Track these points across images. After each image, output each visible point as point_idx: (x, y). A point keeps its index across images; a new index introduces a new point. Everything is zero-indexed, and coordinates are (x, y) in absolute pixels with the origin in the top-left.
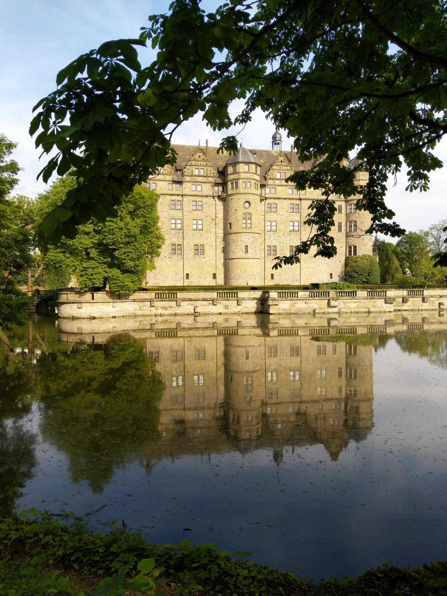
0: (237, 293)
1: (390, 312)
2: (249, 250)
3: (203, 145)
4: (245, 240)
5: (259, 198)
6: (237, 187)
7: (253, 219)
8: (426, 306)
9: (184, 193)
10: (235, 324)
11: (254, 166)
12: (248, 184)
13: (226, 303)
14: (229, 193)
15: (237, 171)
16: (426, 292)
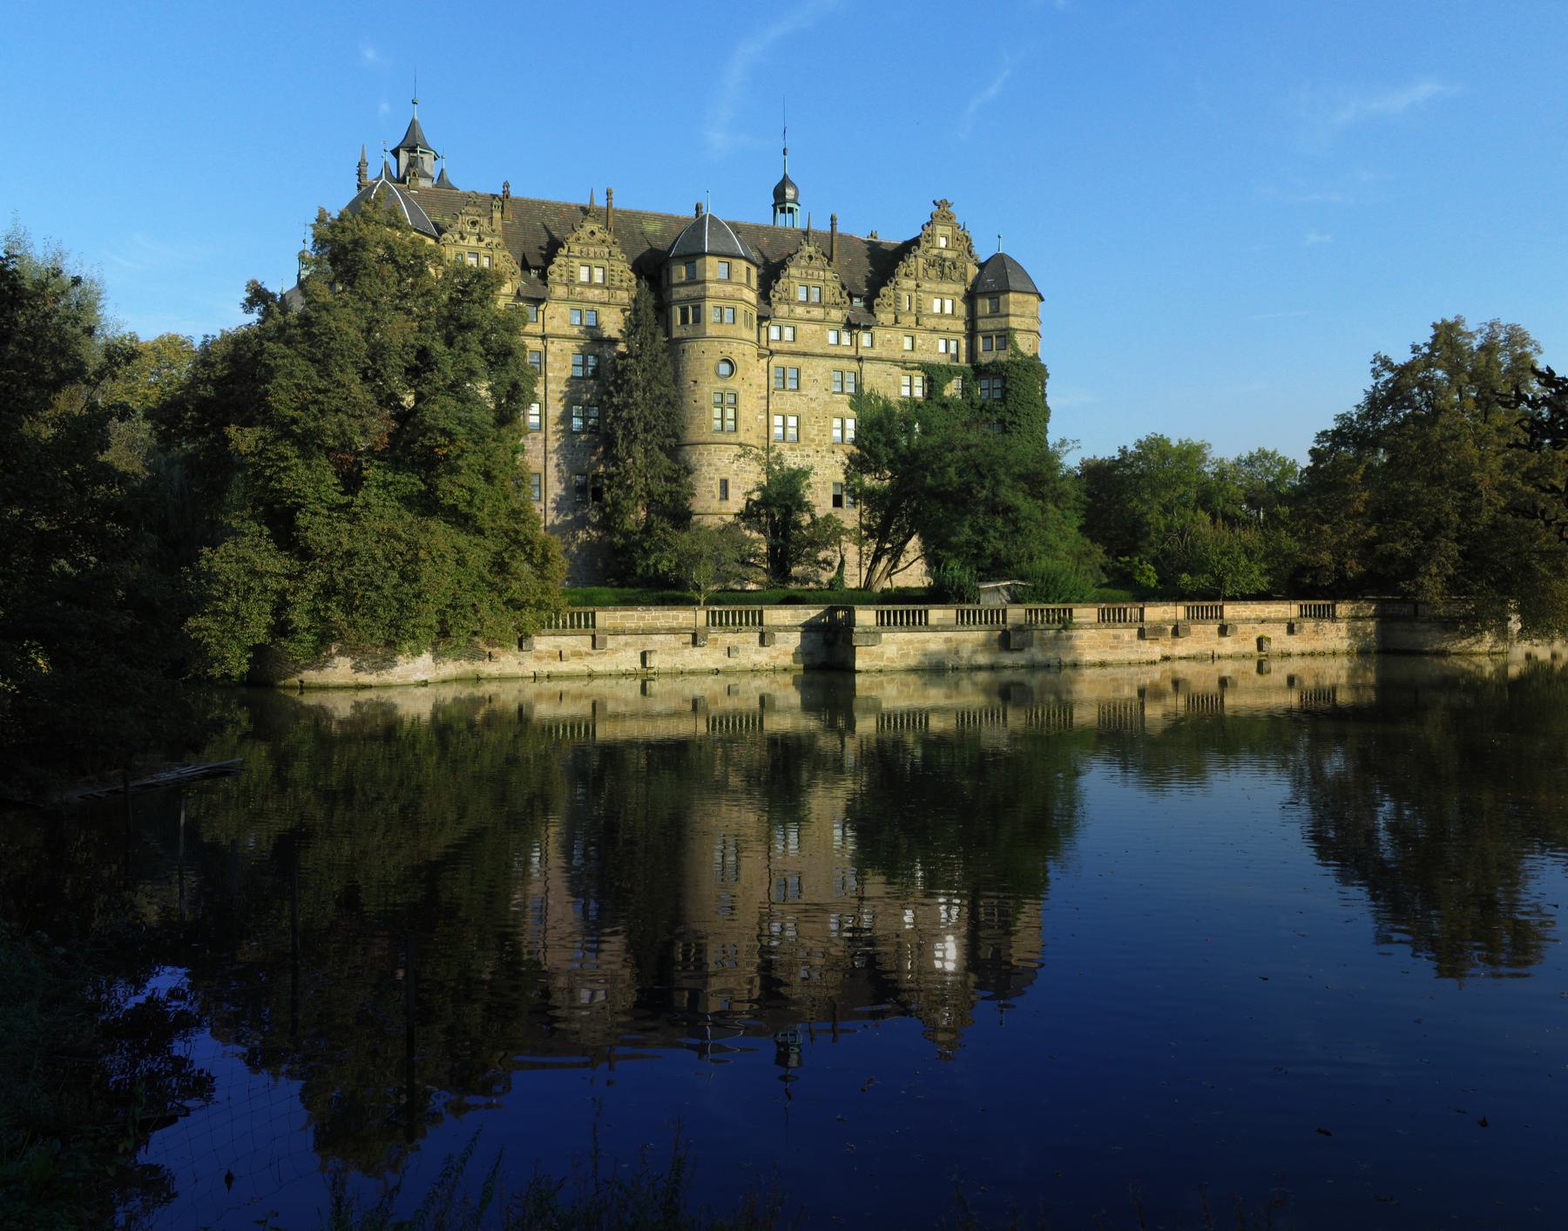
0: (761, 613)
1: (1153, 663)
2: (731, 490)
3: (600, 202)
4: (718, 463)
6: (697, 320)
8: (1228, 645)
9: (548, 330)
10: (755, 704)
11: (744, 264)
12: (728, 313)
13: (730, 639)
15: (699, 278)
16: (1231, 611)
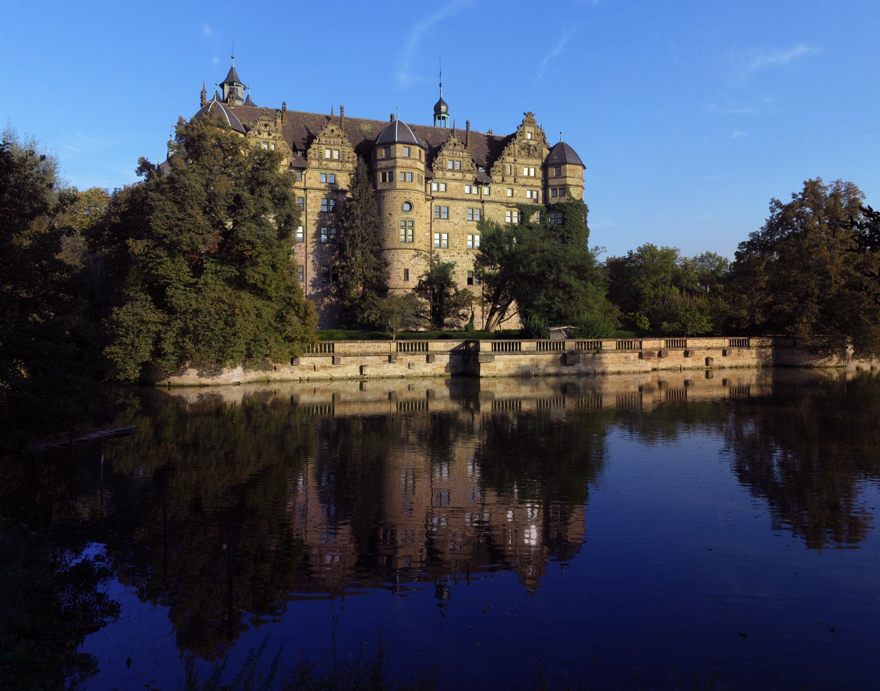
0: (427, 344)
1: (647, 372)
2: (410, 275)
3: (337, 113)
5: (423, 197)
6: (391, 179)
7: (416, 229)
8: (689, 362)
9: (308, 185)
11: (418, 148)
12: (408, 176)
13: (410, 358)
15: (392, 156)
16: (691, 343)
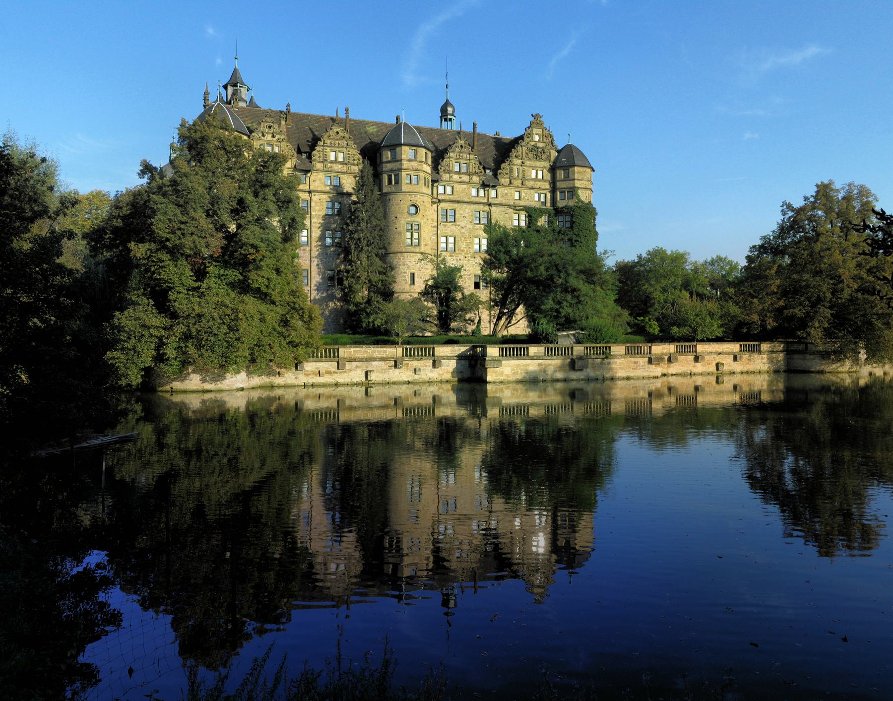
0: (433, 349)
1: (657, 377)
2: (416, 279)
3: (342, 115)
4: (409, 264)
6: (397, 182)
7: (422, 233)
8: (699, 368)
9: (312, 188)
10: (430, 401)
11: (424, 150)
12: (414, 178)
13: (416, 364)
14: (384, 191)
15: (398, 158)
16: (701, 348)
